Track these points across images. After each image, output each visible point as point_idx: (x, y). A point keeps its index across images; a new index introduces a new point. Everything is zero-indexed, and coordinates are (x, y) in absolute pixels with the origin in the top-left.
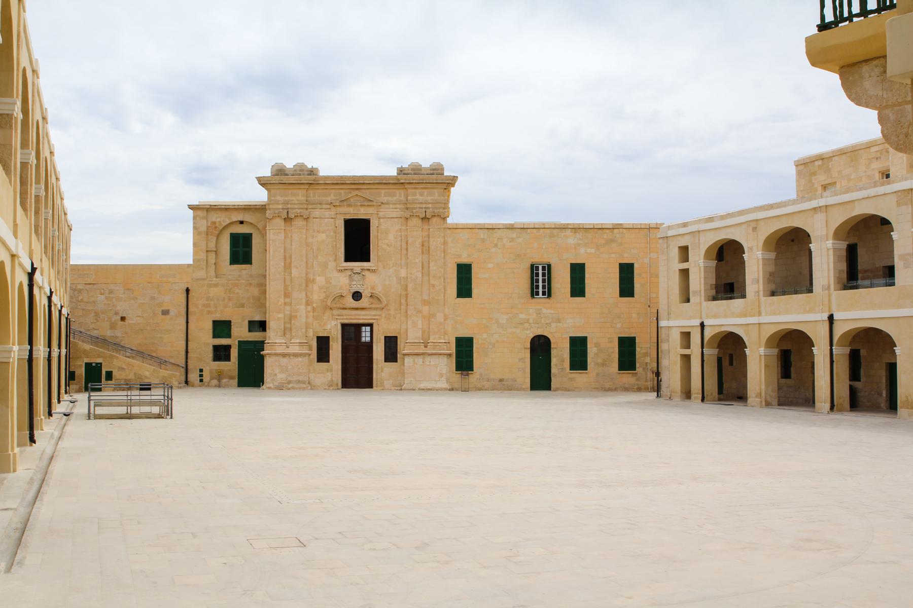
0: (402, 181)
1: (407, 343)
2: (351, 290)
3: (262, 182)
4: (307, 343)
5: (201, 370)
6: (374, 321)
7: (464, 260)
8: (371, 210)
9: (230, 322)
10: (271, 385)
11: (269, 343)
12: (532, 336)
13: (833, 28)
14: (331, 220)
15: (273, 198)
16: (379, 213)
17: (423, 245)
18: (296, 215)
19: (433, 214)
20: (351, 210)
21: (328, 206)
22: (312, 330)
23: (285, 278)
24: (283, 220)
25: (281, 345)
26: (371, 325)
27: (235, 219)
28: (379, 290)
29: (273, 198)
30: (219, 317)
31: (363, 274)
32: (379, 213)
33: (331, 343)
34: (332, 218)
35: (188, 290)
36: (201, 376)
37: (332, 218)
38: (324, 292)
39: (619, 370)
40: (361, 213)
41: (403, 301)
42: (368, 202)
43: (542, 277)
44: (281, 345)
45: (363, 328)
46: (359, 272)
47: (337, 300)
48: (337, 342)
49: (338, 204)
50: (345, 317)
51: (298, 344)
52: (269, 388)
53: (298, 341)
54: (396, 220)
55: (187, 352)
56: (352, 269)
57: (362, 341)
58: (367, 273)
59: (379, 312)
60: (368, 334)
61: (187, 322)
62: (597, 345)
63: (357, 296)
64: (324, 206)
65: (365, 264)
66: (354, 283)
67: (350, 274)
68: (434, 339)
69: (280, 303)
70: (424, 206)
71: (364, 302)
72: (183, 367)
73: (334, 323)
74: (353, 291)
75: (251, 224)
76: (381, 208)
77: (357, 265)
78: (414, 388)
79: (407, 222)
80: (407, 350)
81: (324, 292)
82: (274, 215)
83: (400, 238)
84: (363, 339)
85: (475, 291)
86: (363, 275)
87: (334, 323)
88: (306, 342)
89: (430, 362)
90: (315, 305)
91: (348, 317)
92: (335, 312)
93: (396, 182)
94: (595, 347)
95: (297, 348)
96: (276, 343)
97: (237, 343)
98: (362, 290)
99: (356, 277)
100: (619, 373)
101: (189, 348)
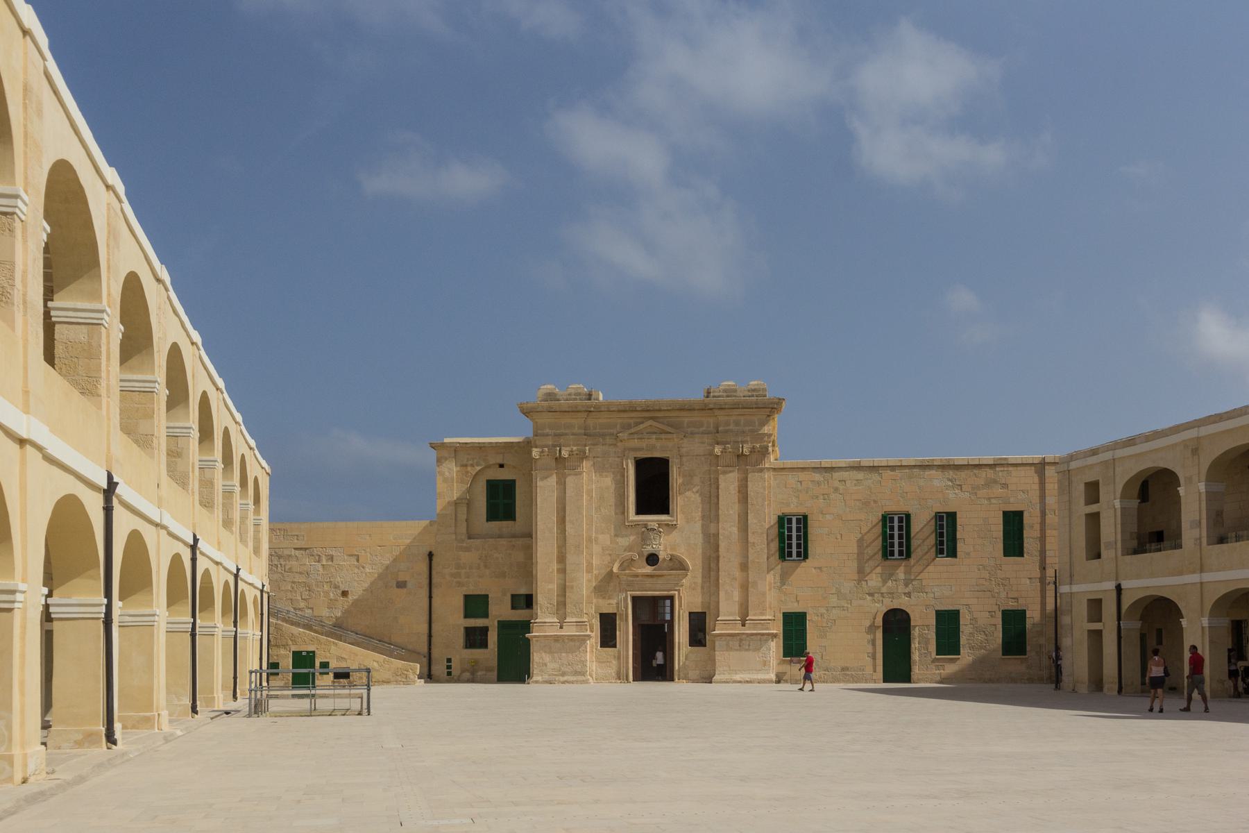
5: (449, 660)
9: (487, 596)
10: (539, 678)
30: (472, 590)
35: (431, 555)
36: (449, 667)
38: (610, 555)
52: (537, 682)
53: (574, 620)
55: (430, 636)
61: (430, 597)
65: (663, 517)
68: (754, 615)
74: (646, 554)
77: (652, 519)
80: (718, 630)
81: (610, 555)
89: (749, 645)
96: (545, 623)
97: (496, 624)
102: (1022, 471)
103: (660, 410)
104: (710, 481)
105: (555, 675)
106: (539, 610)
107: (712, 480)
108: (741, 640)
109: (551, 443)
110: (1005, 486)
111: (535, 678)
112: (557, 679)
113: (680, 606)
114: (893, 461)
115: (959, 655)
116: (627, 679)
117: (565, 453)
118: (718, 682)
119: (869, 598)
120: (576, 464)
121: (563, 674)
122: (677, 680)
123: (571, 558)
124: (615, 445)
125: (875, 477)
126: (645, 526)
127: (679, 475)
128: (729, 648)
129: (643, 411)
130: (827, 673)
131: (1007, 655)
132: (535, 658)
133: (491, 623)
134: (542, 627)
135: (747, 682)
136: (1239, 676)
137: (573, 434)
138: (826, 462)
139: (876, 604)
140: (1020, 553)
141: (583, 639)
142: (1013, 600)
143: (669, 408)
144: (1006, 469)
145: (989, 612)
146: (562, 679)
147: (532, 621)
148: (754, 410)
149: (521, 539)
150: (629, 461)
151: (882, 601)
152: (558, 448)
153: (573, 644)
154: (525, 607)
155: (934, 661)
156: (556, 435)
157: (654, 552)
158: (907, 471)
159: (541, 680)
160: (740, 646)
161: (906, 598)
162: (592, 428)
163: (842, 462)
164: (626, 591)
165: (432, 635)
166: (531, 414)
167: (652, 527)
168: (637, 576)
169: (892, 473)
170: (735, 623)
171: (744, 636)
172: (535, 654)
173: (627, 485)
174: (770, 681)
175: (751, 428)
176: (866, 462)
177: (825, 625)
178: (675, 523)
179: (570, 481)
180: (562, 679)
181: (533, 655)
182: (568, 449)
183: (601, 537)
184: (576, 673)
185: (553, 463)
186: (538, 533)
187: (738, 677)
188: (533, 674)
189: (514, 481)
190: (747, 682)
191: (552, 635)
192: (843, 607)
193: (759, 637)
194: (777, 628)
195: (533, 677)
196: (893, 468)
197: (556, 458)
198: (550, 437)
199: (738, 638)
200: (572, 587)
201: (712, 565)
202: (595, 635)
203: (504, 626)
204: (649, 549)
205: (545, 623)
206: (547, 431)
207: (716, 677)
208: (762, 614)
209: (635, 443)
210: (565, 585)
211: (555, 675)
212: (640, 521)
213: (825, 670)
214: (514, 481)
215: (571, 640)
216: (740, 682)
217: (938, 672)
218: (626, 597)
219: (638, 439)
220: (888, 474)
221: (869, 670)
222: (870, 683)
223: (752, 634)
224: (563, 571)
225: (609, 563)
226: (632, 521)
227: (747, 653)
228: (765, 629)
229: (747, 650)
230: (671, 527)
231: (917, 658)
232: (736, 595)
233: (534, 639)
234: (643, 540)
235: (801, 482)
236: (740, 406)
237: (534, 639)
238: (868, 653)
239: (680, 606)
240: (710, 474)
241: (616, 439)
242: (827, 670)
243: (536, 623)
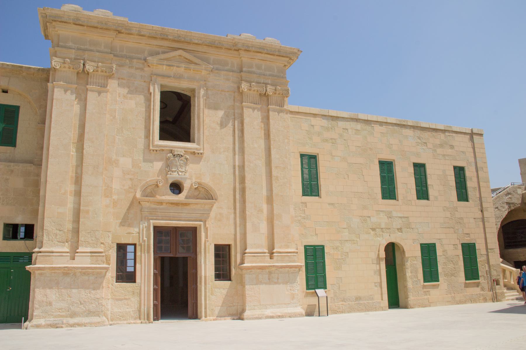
7: (309, 150)
10: (42, 322)
12: (386, 244)
25: (62, 256)
26: (135, 245)
38: (131, 179)
43: (220, 258)
44: (62, 256)
45: (128, 246)
46: (182, 154)
48: (149, 252)
51: (90, 254)
52: (38, 326)
53: (89, 250)
68: (280, 248)
74: (170, 181)
78: (260, 316)
80: (248, 263)
81: (131, 179)
83: (233, 117)
89: (278, 279)
95: (88, 259)
96: (53, 252)
102: (459, 138)
103: (189, 43)
104: (234, 115)
105: (62, 316)
106: (45, 237)
107: (236, 115)
108: (270, 273)
109: (73, 57)
110: (452, 147)
111: (35, 322)
112: (65, 321)
113: (207, 237)
114: (380, 119)
115: (438, 281)
116: (148, 319)
117: (90, 67)
118: (250, 319)
119: (372, 233)
121: (73, 315)
122: (203, 318)
123: (87, 179)
124: (142, 69)
125: (368, 128)
126: (171, 152)
127: (205, 107)
128: (259, 282)
129: (174, 41)
130: (344, 303)
132: (36, 295)
134: (48, 258)
135: (279, 317)
137: (99, 51)
138: (333, 113)
139: (378, 238)
140: (218, 248)
141: (100, 274)
142: (467, 236)
143: (200, 42)
144: (451, 134)
145: (454, 245)
146: (72, 321)
147: (36, 250)
148: (275, 57)
149: (21, 165)
150: (156, 86)
151: (382, 235)
152: (82, 62)
153: (86, 278)
155: (424, 287)
156: (79, 49)
157: (180, 180)
158: (391, 127)
160: (269, 279)
161: (399, 233)
162: (118, 52)
163: (345, 114)
164: (149, 220)
166: (54, 23)
167: (179, 153)
168: (161, 203)
169: (380, 127)
170: (264, 256)
171: (273, 269)
172: (37, 290)
173: (154, 109)
174: (301, 315)
175: (271, 73)
176: (362, 116)
177: (340, 257)
178: (201, 151)
179: (92, 97)
180: (72, 321)
181: (34, 291)
182: (95, 64)
183: (122, 160)
184: (90, 313)
185: (74, 78)
186: (51, 148)
187: (269, 312)
188: (32, 315)
189: (18, 108)
190: (279, 317)
191: (60, 267)
192: (353, 240)
193: (287, 269)
194: (301, 261)
195: (32, 319)
196: (381, 123)
197: (78, 73)
198: (74, 51)
199: (267, 270)
200: (87, 212)
204: (174, 177)
205: (53, 252)
206: (70, 44)
207: (247, 314)
208: (287, 247)
209: (164, 69)
210: (79, 209)
211: (62, 316)
212: (166, 147)
213: (342, 301)
214: (18, 108)
215: (85, 273)
216: (272, 317)
217: (426, 297)
219: (167, 65)
220: (377, 127)
221: (377, 297)
222: (378, 310)
223: (282, 267)
224: (78, 194)
225: (130, 188)
226: (157, 146)
227: (275, 286)
228: (290, 262)
229: (276, 283)
230: (197, 155)
231: (411, 286)
232: (264, 227)
233: (37, 272)
234: (168, 166)
235: (313, 126)
236: (265, 51)
237: (37, 272)
238: (375, 283)
239: (207, 237)
240: (234, 109)
241: (143, 64)
242: (344, 300)
243: (40, 252)
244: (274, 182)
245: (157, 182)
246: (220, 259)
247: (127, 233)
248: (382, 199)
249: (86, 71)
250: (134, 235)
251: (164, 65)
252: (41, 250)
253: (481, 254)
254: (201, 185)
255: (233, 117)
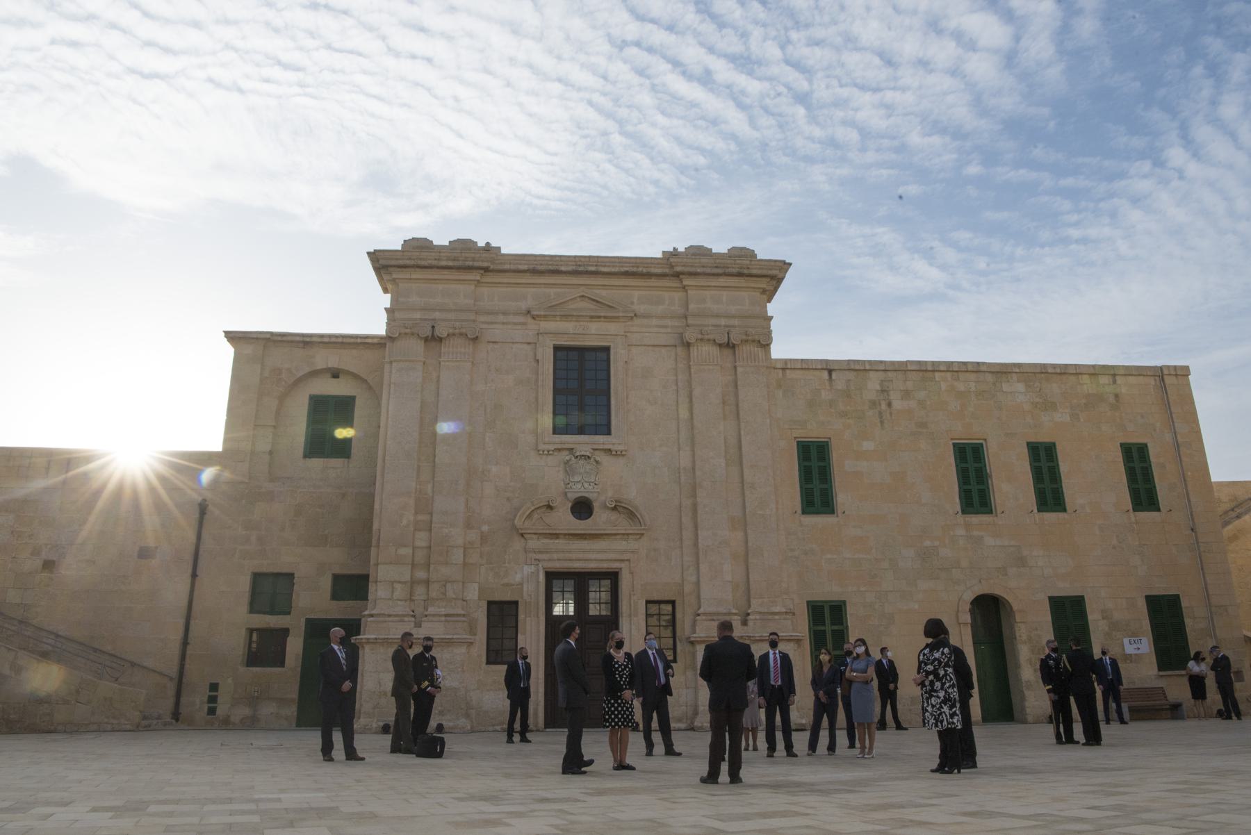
0: (678, 269)
1: (699, 615)
2: (569, 495)
3: (381, 262)
4: (464, 615)
5: (214, 687)
6: (622, 565)
7: (814, 432)
8: (613, 328)
9: (292, 575)
11: (372, 616)
13: (354, 689)
14: (526, 346)
15: (401, 299)
16: (628, 334)
17: (724, 403)
18: (451, 331)
19: (744, 337)
20: (569, 326)
21: (521, 319)
22: (476, 586)
23: (419, 467)
24: (423, 342)
26: (673, 603)
27: (320, 364)
28: (632, 494)
29: (401, 299)
31: (598, 459)
32: (628, 334)
33: (521, 617)
34: (529, 343)
36: (213, 699)
37: (529, 343)
39: (1160, 670)
40: (592, 334)
41: (686, 520)
42: (605, 311)
46: (588, 454)
47: (536, 516)
49: (542, 313)
50: (555, 556)
51: (443, 619)
53: (443, 611)
54: (663, 350)
55: (185, 643)
56: (572, 449)
57: (554, 614)
58: (600, 457)
59: (633, 545)
60: (605, 596)
62: (1105, 615)
63: (582, 508)
64: (511, 318)
65: (600, 439)
66: (577, 478)
67: (567, 458)
69: (405, 522)
70: (723, 322)
71: (601, 519)
72: (171, 679)
73: (528, 570)
74: (572, 496)
75: (365, 381)
76: (632, 326)
77: (583, 443)
79: (689, 350)
82: (403, 331)
84: (591, 613)
85: (842, 498)
86: (597, 462)
87: (528, 570)
88: (463, 612)
90: (485, 528)
91: (561, 556)
92: (534, 543)
93: (667, 271)
94: (1103, 618)
98: (595, 495)
99: (582, 466)
100: (1162, 676)
101: (191, 635)
104: (677, 384)
120: (463, 350)
131: (1165, 670)
133: (295, 624)
136: (973, 688)
154: (365, 602)
159: (691, 363)
165: (189, 641)
167: (583, 453)
201: (684, 519)
202: (842, 465)
203: (317, 630)
218: (538, 571)
244: (747, 493)
245: (549, 502)
246: (828, 621)
247: (503, 585)
248: (1082, 597)
249: (436, 337)
250: (514, 587)
251: (676, 375)
252: (372, 612)
253: (379, 566)
254: (620, 502)
255: (675, 388)
